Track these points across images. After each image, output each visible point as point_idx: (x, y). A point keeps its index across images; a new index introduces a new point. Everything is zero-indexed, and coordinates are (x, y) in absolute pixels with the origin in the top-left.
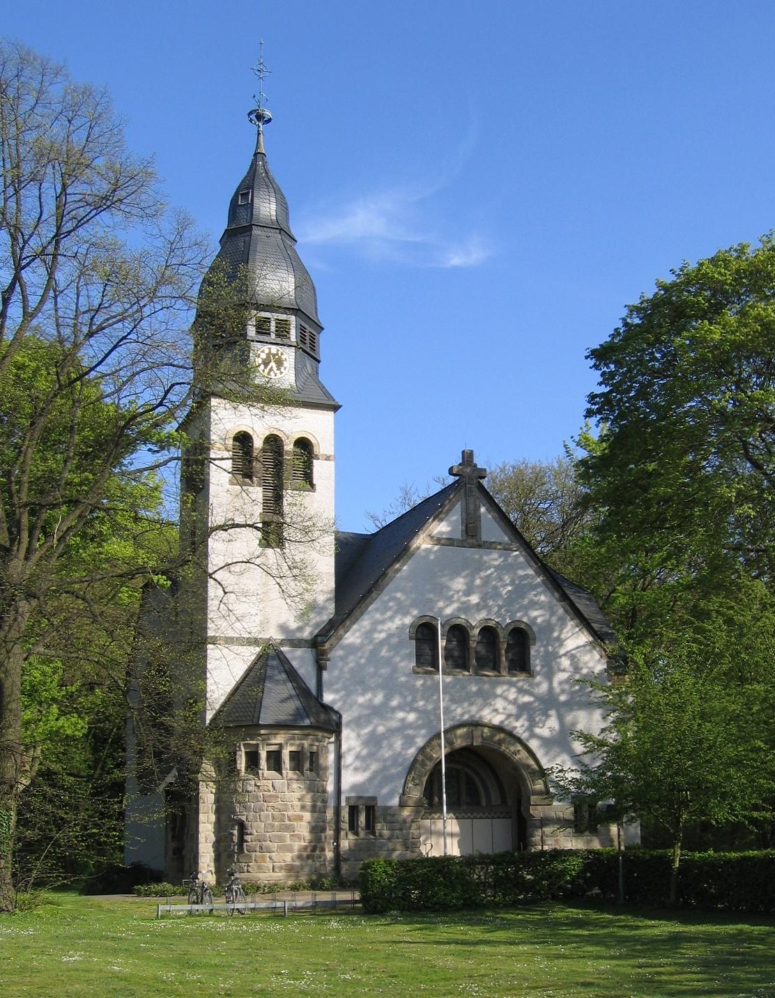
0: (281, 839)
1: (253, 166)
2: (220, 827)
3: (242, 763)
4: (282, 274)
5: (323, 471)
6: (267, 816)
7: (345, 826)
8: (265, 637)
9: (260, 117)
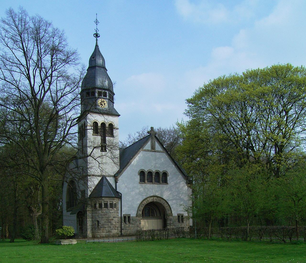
7: (123, 221)
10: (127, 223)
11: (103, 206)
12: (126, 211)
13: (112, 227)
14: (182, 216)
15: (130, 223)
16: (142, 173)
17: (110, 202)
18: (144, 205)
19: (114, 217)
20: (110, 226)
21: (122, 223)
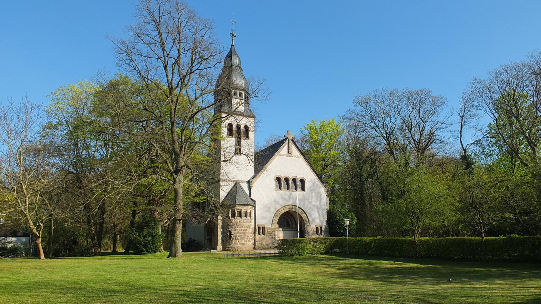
0: (241, 236)
1: (231, 49)
2: (223, 233)
3: (230, 215)
4: (240, 80)
5: (251, 134)
6: (237, 229)
7: (257, 232)
8: (236, 180)
9: (233, 35)
10: (261, 234)
11: (236, 215)
12: (260, 222)
13: (245, 238)
14: (263, 228)
15: (264, 235)
16: (278, 179)
17: (244, 210)
18: (280, 215)
19: (248, 228)
20: (243, 237)
21: (256, 234)
